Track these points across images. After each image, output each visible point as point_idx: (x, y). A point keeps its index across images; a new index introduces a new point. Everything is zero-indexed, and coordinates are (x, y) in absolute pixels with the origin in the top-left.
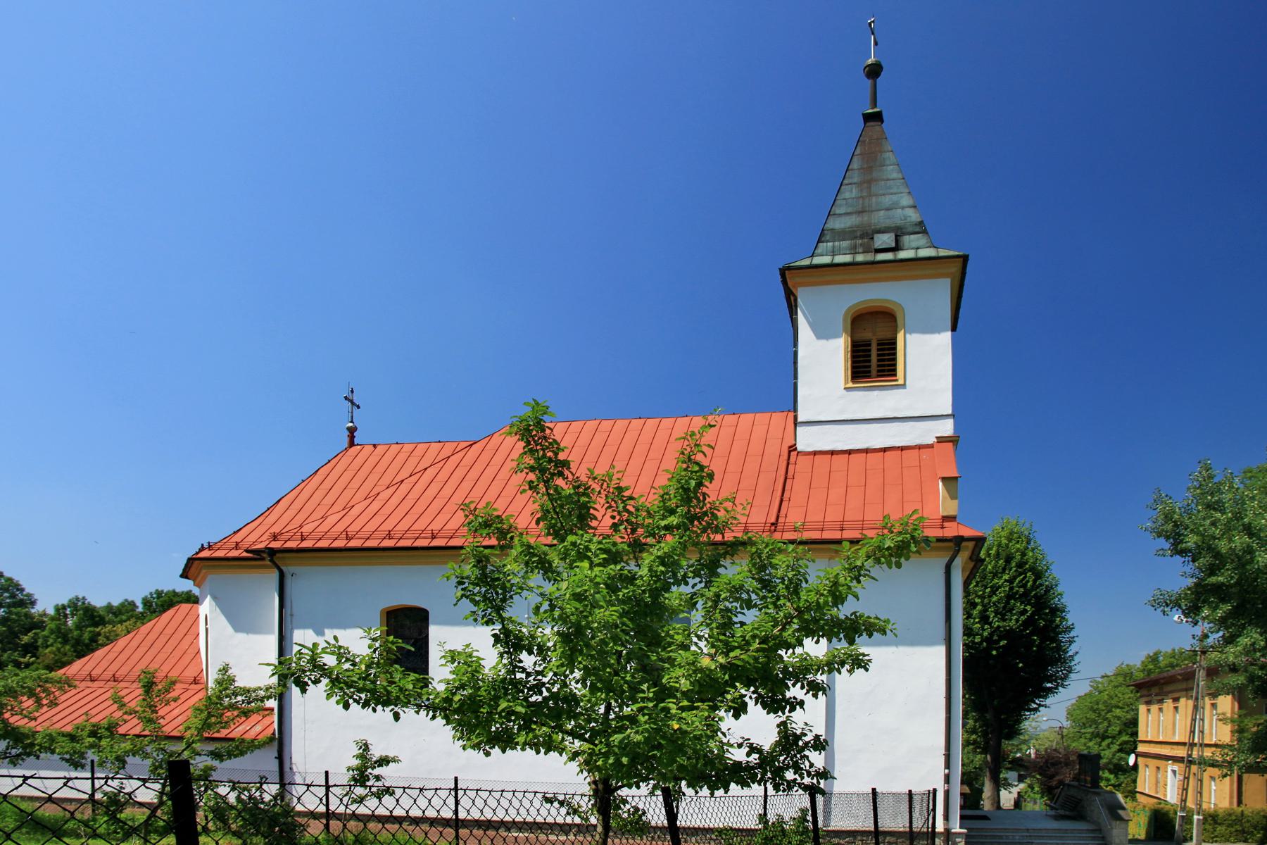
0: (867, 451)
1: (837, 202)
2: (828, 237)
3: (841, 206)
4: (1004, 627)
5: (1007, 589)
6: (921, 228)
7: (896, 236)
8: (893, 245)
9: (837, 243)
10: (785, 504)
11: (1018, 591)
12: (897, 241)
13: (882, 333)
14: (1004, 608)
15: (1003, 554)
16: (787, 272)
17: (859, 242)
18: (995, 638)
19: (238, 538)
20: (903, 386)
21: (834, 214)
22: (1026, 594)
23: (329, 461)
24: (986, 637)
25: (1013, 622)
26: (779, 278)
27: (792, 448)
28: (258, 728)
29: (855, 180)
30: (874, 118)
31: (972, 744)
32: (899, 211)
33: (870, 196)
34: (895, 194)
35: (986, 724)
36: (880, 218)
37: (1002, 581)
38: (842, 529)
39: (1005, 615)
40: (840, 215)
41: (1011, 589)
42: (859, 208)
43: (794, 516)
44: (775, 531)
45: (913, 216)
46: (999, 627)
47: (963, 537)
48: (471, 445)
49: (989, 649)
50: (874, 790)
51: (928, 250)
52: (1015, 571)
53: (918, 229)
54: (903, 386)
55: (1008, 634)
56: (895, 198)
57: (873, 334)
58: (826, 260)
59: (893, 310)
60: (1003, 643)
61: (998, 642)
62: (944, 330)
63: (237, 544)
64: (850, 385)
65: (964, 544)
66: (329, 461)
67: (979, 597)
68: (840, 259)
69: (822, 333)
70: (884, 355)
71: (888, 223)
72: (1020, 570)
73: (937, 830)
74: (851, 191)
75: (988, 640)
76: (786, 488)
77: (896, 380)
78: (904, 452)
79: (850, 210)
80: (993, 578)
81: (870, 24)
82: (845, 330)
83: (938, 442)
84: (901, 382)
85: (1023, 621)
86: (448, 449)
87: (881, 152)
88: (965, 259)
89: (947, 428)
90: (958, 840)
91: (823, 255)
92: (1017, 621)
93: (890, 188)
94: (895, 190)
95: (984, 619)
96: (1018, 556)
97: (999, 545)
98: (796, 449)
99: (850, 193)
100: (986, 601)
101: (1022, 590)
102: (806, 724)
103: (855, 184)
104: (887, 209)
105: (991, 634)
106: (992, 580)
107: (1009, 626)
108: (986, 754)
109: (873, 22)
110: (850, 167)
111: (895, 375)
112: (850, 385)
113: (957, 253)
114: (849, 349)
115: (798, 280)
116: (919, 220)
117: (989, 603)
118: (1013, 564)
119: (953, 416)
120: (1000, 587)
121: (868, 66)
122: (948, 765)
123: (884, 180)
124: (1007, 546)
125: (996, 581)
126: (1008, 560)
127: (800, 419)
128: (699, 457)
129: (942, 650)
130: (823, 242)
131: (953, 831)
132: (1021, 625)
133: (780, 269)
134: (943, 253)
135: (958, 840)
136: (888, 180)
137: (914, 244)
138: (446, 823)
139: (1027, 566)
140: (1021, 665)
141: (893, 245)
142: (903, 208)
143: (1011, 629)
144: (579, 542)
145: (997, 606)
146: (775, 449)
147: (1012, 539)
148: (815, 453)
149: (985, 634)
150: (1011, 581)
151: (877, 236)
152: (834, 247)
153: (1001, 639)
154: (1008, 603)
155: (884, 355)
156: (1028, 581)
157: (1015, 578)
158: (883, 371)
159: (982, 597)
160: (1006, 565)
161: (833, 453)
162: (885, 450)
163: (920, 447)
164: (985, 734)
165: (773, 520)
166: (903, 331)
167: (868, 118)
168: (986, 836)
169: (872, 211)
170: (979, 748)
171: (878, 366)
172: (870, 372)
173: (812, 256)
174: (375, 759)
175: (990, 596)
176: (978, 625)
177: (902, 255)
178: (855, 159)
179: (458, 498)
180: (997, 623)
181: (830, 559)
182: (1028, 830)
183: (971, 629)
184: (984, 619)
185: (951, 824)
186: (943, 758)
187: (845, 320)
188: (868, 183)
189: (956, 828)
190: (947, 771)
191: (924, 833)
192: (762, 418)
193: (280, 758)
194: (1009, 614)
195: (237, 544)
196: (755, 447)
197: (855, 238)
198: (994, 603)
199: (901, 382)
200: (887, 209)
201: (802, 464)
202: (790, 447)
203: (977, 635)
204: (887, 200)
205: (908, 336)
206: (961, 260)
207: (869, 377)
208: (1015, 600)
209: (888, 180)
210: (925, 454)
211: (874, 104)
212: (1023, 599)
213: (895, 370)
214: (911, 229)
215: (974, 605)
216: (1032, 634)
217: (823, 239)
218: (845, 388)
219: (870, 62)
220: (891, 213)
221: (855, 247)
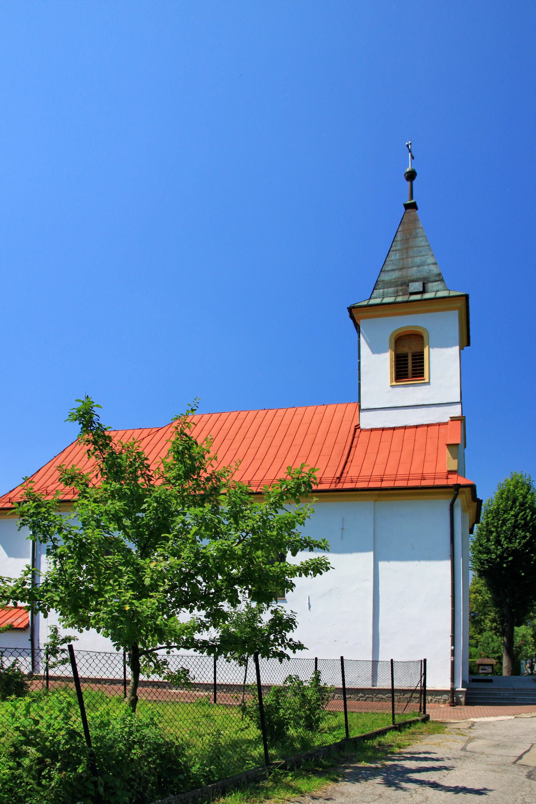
0: (405, 428)
1: (387, 263)
2: (380, 286)
3: (389, 265)
4: (511, 547)
5: (513, 521)
6: (439, 278)
7: (424, 284)
8: (421, 289)
9: (385, 290)
10: (348, 464)
11: (520, 523)
12: (424, 287)
13: (415, 349)
14: (511, 534)
15: (511, 498)
16: (352, 310)
17: (400, 288)
18: (505, 555)
19: (11, 495)
20: (429, 383)
21: (384, 271)
22: (526, 524)
23: (72, 443)
24: (499, 555)
25: (517, 544)
26: (348, 314)
27: (357, 427)
28: (20, 620)
29: (398, 248)
30: (409, 207)
31: (494, 630)
32: (426, 267)
33: (407, 258)
34: (423, 256)
35: (502, 615)
36: (413, 272)
37: (510, 516)
38: (382, 481)
39: (511, 539)
40: (388, 271)
41: (516, 521)
42: (400, 266)
43: (352, 472)
44: (339, 482)
45: (435, 270)
46: (507, 548)
47: (459, 484)
48: (158, 430)
49: (501, 563)
50: (392, 660)
51: (444, 292)
52: (519, 509)
53: (437, 279)
54: (429, 383)
55: (514, 553)
56: (423, 258)
57: (408, 349)
58: (378, 301)
59: (418, 332)
60: (510, 558)
61: (507, 558)
62: (455, 345)
63: (10, 499)
64: (394, 383)
65: (461, 490)
66: (72, 443)
67: (494, 527)
68: (387, 300)
69: (376, 350)
70: (416, 363)
71: (419, 275)
72: (522, 508)
73: (427, 689)
74: (396, 254)
75: (500, 557)
76: (351, 454)
77: (424, 380)
78: (429, 428)
79: (394, 267)
80: (504, 514)
81: (408, 146)
82: (391, 348)
83: (451, 421)
84: (427, 381)
85: (524, 544)
86: (146, 432)
87: (415, 229)
88: (467, 297)
89: (456, 411)
90: (460, 696)
91: (376, 298)
92: (520, 543)
93: (420, 252)
94: (423, 253)
95: (498, 542)
96: (521, 499)
97: (509, 491)
98: (359, 428)
99: (394, 256)
100: (499, 529)
101: (523, 522)
102: (292, 612)
103: (398, 250)
104: (418, 266)
105: (503, 553)
106: (503, 515)
107: (514, 547)
108: (503, 636)
109: (410, 144)
110: (395, 239)
111: (423, 376)
112: (394, 383)
113: (461, 293)
114: (393, 360)
115: (359, 315)
116: (438, 272)
117: (501, 531)
118: (518, 504)
119: (461, 402)
120: (508, 520)
121: (407, 173)
122: (453, 643)
123: (416, 247)
124: (514, 491)
125: (506, 516)
126: (514, 502)
127: (362, 408)
128: (187, 431)
129: (448, 563)
130: (377, 289)
131: (457, 689)
132: (522, 546)
133: (348, 308)
134: (452, 294)
135: (460, 696)
136: (419, 247)
137: (435, 289)
138: (205, 687)
139: (527, 505)
140: (523, 574)
141: (421, 289)
142: (428, 265)
143: (516, 548)
144: (109, 488)
145: (507, 533)
146: (347, 428)
147: (517, 487)
148: (372, 430)
149: (499, 552)
150: (516, 516)
151: (410, 284)
152: (384, 292)
153: (509, 556)
154: (514, 531)
155: (416, 363)
156: (527, 516)
157: (519, 513)
158: (417, 373)
159: (496, 527)
160: (512, 505)
161: (383, 429)
162: (417, 427)
163: (439, 424)
164: (502, 623)
165: (338, 475)
166: (427, 347)
167: (408, 207)
168: (486, 694)
169: (409, 268)
170: (499, 632)
171: (413, 370)
172: (407, 374)
173: (370, 299)
174: (61, 638)
175: (502, 527)
176: (494, 547)
177: (427, 296)
178: (398, 234)
179: (57, 464)
180: (506, 545)
181: (375, 501)
182: (514, 689)
183: (490, 549)
184: (498, 542)
185: (456, 685)
186: (450, 639)
187: (390, 340)
188: (407, 248)
189: (460, 688)
190: (452, 647)
191: (418, 690)
192: (341, 407)
193: (32, 640)
194: (514, 538)
195: (10, 499)
196: (334, 428)
197: (397, 286)
198: (504, 531)
199: (427, 381)
200: (418, 266)
201: (363, 437)
202: (356, 426)
203: (493, 553)
204: (418, 260)
205: (431, 350)
206: (464, 298)
207: (407, 378)
208: (519, 529)
209: (419, 247)
210: (442, 429)
211: (412, 197)
212: (525, 528)
213: (423, 373)
214: (433, 279)
215: (491, 532)
216: (530, 552)
217: (377, 287)
218: (391, 386)
219: (408, 170)
220: (421, 268)
221: (397, 292)
